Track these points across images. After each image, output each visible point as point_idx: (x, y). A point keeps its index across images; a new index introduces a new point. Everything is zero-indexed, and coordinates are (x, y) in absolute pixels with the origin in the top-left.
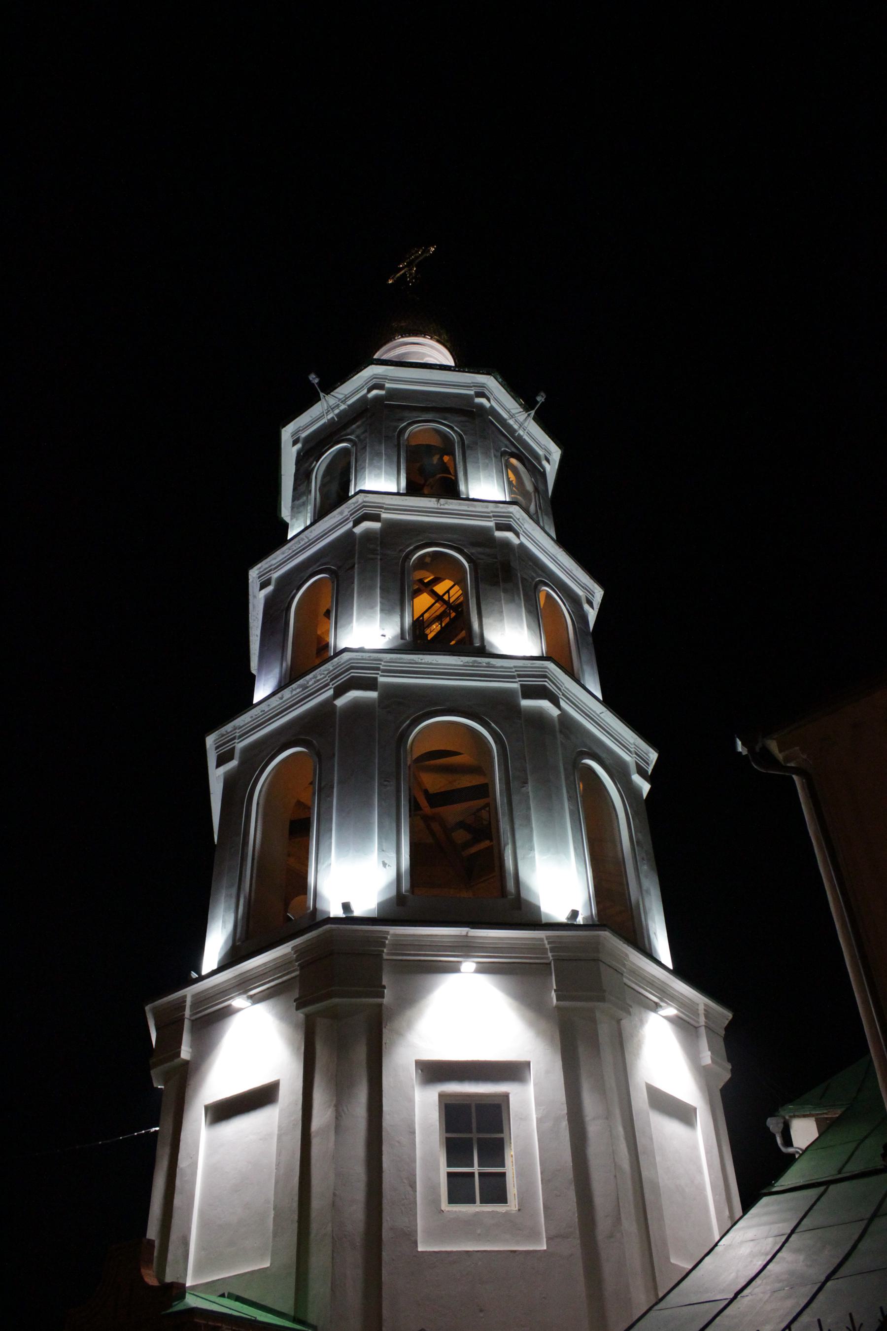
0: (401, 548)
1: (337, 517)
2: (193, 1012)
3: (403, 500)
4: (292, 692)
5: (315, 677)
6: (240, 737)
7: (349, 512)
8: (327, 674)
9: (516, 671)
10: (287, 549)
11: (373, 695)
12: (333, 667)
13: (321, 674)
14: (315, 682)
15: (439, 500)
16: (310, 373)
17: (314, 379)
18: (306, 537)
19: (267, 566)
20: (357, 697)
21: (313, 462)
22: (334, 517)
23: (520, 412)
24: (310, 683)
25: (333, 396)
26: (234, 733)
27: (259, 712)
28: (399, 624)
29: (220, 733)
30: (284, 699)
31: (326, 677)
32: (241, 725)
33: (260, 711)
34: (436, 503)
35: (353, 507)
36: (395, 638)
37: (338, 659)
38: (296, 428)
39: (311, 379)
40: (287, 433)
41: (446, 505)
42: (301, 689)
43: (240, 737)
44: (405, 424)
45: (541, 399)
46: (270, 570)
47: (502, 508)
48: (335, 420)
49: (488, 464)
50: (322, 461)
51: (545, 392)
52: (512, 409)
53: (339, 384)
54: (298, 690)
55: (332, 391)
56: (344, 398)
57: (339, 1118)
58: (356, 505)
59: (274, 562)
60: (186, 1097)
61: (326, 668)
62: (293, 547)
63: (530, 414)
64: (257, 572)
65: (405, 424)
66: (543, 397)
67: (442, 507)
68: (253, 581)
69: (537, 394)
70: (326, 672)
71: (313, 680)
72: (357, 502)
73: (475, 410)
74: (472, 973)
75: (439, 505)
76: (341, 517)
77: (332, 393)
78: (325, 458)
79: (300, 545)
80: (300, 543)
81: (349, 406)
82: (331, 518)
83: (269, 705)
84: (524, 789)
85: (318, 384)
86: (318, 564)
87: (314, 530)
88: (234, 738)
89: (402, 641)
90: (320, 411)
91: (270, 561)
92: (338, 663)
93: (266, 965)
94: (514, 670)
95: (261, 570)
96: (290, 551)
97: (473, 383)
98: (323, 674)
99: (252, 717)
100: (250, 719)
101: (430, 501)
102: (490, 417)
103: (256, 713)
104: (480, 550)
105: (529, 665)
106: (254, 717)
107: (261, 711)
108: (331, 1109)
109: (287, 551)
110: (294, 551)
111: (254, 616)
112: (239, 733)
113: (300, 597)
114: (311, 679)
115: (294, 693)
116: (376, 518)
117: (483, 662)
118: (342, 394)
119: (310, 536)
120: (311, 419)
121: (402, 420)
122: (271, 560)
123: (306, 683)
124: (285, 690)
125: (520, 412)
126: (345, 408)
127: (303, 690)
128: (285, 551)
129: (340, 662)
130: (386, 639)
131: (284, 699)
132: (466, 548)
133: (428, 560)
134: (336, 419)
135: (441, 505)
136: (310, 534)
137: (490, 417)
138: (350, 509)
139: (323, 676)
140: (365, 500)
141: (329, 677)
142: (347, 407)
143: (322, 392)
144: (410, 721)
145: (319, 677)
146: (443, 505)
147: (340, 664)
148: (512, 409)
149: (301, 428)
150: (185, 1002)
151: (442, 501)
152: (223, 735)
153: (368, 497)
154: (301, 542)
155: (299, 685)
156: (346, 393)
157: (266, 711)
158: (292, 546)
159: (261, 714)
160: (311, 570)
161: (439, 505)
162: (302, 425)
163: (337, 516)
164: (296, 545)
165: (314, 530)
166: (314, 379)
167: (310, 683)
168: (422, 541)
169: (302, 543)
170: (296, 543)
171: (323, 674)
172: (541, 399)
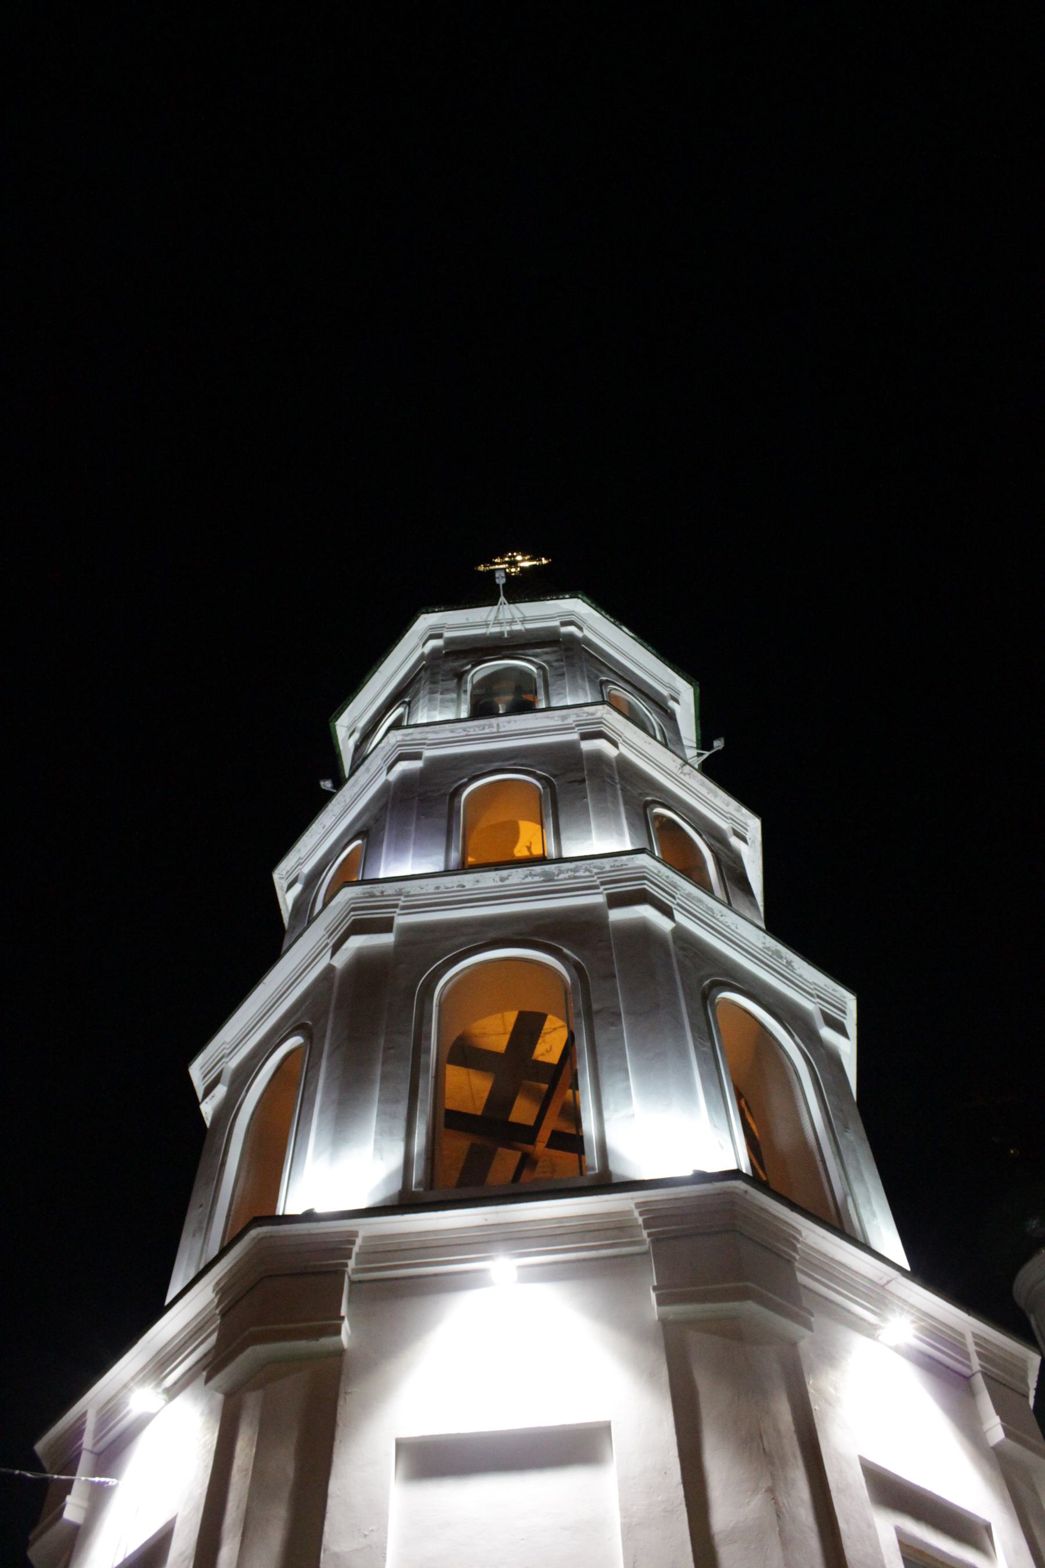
1: (555, 721)
2: (360, 1266)
3: (645, 742)
4: (526, 877)
5: (575, 870)
6: (404, 908)
7: (574, 721)
8: (597, 874)
10: (460, 728)
12: (611, 867)
13: (587, 870)
14: (570, 878)
15: (684, 765)
18: (498, 725)
19: (418, 736)
21: (467, 665)
22: (553, 718)
24: (561, 876)
27: (455, 885)
29: (369, 890)
30: (506, 882)
31: (593, 876)
32: (412, 893)
33: (458, 883)
34: (679, 766)
35: (583, 718)
37: (627, 859)
38: (441, 622)
40: (426, 622)
41: (687, 776)
42: (542, 879)
43: (404, 908)
45: (718, 744)
46: (424, 744)
47: (742, 815)
48: (504, 635)
50: (482, 669)
51: (726, 743)
52: (686, 739)
53: (526, 600)
54: (537, 879)
56: (510, 620)
57: (781, 1516)
58: (590, 717)
59: (431, 736)
60: (338, 1415)
61: (602, 863)
62: (471, 730)
63: (702, 754)
64: (399, 738)
67: (682, 776)
68: (384, 747)
69: (717, 737)
70: (595, 871)
71: (570, 874)
72: (593, 714)
74: (891, 1348)
75: (680, 771)
76: (560, 723)
78: (487, 667)
79: (481, 732)
80: (484, 729)
81: (527, 630)
82: (548, 717)
83: (478, 881)
86: (513, 762)
87: (515, 721)
88: (396, 906)
90: (482, 619)
91: (427, 733)
92: (622, 865)
93: (563, 1222)
94: (812, 987)
96: (464, 733)
98: (590, 871)
99: (438, 888)
100: (432, 891)
101: (674, 761)
103: (449, 885)
106: (442, 889)
107: (458, 886)
108: (759, 1496)
109: (461, 731)
110: (467, 735)
111: (344, 796)
112: (404, 902)
113: (475, 789)
114: (568, 870)
115: (529, 879)
117: (786, 958)
118: (522, 613)
119: (504, 727)
120: (465, 621)
122: (430, 732)
123: (556, 873)
124: (519, 870)
126: (521, 630)
127: (544, 881)
128: (457, 729)
129: (626, 865)
131: (506, 882)
134: (506, 636)
135: (681, 773)
136: (506, 724)
138: (578, 719)
139: (587, 874)
140: (604, 716)
141: (599, 878)
142: (523, 629)
143: (504, 596)
144: (710, 982)
145: (581, 873)
146: (685, 774)
147: (624, 867)
148: (686, 739)
149: (447, 626)
150: (353, 1243)
152: (372, 896)
153: (611, 715)
154: (487, 727)
155: (545, 871)
156: (527, 615)
157: (467, 888)
158: (470, 727)
159: (455, 889)
160: (496, 765)
161: (680, 771)
162: (449, 623)
163: (556, 718)
164: (477, 729)
165: (515, 721)
167: (561, 876)
168: (660, 798)
169: (487, 731)
170: (478, 726)
171: (590, 871)
172: (718, 744)
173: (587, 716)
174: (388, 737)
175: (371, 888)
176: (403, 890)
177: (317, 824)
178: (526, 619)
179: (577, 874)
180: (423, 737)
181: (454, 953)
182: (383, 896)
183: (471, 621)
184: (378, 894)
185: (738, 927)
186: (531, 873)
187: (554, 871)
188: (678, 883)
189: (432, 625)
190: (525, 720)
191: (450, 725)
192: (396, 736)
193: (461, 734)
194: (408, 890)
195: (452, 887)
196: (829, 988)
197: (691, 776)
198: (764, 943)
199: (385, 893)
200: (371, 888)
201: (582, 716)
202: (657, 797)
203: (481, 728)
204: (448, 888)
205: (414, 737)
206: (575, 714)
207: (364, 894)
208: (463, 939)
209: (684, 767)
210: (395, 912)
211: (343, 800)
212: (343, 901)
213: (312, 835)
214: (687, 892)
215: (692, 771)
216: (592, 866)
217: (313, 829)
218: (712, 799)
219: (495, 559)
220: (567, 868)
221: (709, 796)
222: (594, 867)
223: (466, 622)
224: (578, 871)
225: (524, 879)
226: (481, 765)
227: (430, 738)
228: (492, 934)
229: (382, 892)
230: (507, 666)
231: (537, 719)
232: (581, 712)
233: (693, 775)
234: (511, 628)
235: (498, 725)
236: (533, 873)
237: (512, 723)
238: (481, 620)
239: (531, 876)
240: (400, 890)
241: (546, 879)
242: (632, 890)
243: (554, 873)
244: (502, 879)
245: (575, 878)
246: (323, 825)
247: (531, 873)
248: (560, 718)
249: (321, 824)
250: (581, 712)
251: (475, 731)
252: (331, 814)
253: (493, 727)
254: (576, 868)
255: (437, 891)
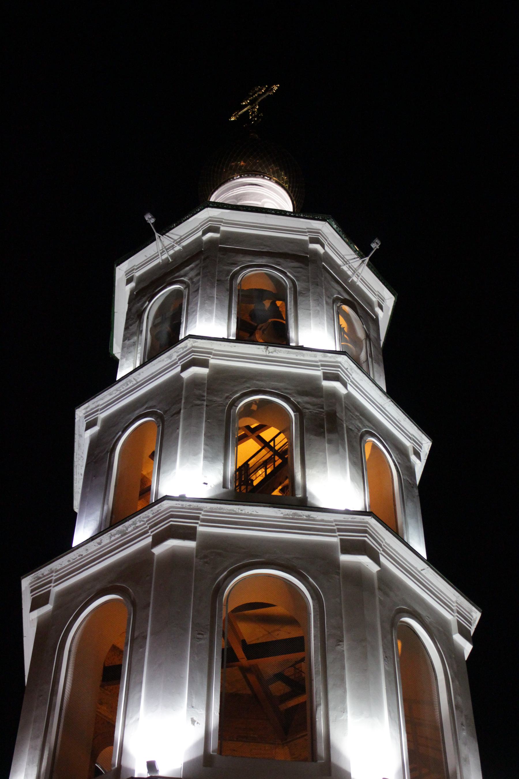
0: (227, 395)
4: (111, 537)
5: (134, 523)
7: (178, 356)
8: (147, 521)
9: (336, 525)
10: (114, 390)
11: (191, 544)
12: (153, 514)
14: (134, 529)
15: (267, 348)
16: (145, 214)
17: (150, 219)
18: (134, 379)
19: (94, 406)
20: (174, 546)
21: (145, 302)
22: (163, 360)
23: (355, 258)
24: (129, 530)
25: (168, 236)
26: (50, 577)
27: (77, 556)
28: (222, 472)
29: (36, 575)
31: (145, 524)
32: (58, 568)
33: (78, 555)
34: (265, 350)
35: (182, 352)
36: (217, 486)
37: (158, 507)
39: (147, 219)
41: (274, 353)
42: (120, 535)
43: (56, 581)
44: (239, 268)
45: (375, 245)
46: (97, 411)
47: (330, 357)
48: (169, 260)
49: (319, 311)
54: (117, 536)
55: (168, 232)
58: (185, 350)
59: (101, 402)
64: (84, 411)
65: (239, 268)
66: (377, 244)
67: (271, 354)
68: (79, 420)
69: (372, 241)
70: (145, 520)
71: (132, 527)
73: (308, 256)
75: (268, 352)
76: (169, 361)
77: (167, 234)
78: (158, 298)
80: (128, 385)
81: (183, 247)
82: (160, 361)
83: (87, 550)
84: (339, 647)
85: (154, 224)
86: (145, 407)
89: (225, 490)
91: (97, 402)
92: (158, 511)
95: (88, 410)
96: (118, 392)
97: (308, 228)
98: (143, 521)
99: (69, 561)
100: (67, 563)
102: (323, 263)
104: (306, 399)
105: (350, 520)
106: (72, 561)
107: (79, 556)
109: (115, 392)
111: (79, 455)
114: (130, 525)
115: (113, 538)
116: (204, 364)
121: (235, 264)
125: (355, 258)
126: (180, 250)
127: (122, 536)
129: (160, 510)
130: (208, 487)
131: (102, 544)
132: (293, 397)
133: (254, 407)
134: (171, 260)
135: (269, 353)
136: (138, 376)
137: (323, 263)
139: (142, 523)
140: (193, 345)
143: (158, 232)
145: (138, 524)
146: (272, 352)
147: (160, 511)
148: (346, 255)
151: (271, 349)
152: (39, 578)
153: (197, 342)
154: (129, 383)
156: (182, 235)
158: (119, 388)
159: (78, 558)
160: (137, 413)
161: (268, 352)
162: (136, 265)
163: (166, 359)
164: (124, 387)
166: (150, 219)
167: (129, 530)
170: (124, 385)
171: (143, 521)
172: (375, 245)
173: (183, 350)
174: (77, 414)
175: (35, 575)
176: (52, 569)
177: (76, 474)
178: (182, 238)
179: (137, 525)
180: (96, 405)
181: (75, 613)
182: (44, 576)
183: (149, 256)
184: (41, 576)
185: (257, 511)
186: (111, 535)
187: (123, 529)
188: (199, 506)
189: (127, 271)
190: (148, 369)
191: (106, 391)
192: (81, 411)
193: (117, 394)
194: (55, 568)
195: (76, 558)
196: (348, 519)
197: (277, 351)
198: (282, 513)
199: (45, 574)
200: (35, 575)
201: (180, 351)
202: (244, 389)
203: (126, 385)
204: (74, 559)
205: (91, 407)
206: (175, 352)
207: (35, 578)
208: (81, 598)
209: (268, 349)
210: (50, 587)
211: (80, 457)
212: (27, 586)
213: (78, 482)
214: (209, 508)
215: (275, 349)
216: (141, 518)
217: (76, 478)
218: (302, 358)
219: (242, 103)
220: (129, 525)
221: (298, 357)
222: (143, 518)
223: (146, 258)
224: (136, 524)
225: (110, 539)
226: (128, 416)
227: (101, 404)
228: (98, 586)
229: (43, 574)
230: (171, 291)
231: (154, 365)
232: (177, 349)
233: (278, 351)
234: (174, 250)
235: (134, 379)
236: (113, 534)
237: (142, 374)
238: (155, 253)
239: (113, 536)
240: (51, 569)
241: (123, 534)
242: (164, 528)
243: (124, 530)
244: (99, 544)
245: (137, 527)
246: (80, 474)
247: (111, 535)
248: (167, 359)
249: (79, 474)
250: (177, 349)
251: (123, 388)
252: (80, 467)
253: (133, 381)
254: (133, 522)
255: (70, 563)
